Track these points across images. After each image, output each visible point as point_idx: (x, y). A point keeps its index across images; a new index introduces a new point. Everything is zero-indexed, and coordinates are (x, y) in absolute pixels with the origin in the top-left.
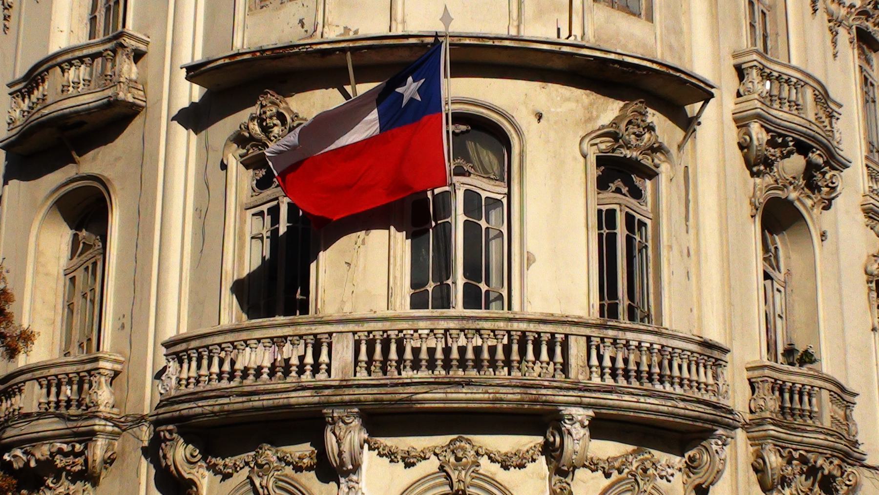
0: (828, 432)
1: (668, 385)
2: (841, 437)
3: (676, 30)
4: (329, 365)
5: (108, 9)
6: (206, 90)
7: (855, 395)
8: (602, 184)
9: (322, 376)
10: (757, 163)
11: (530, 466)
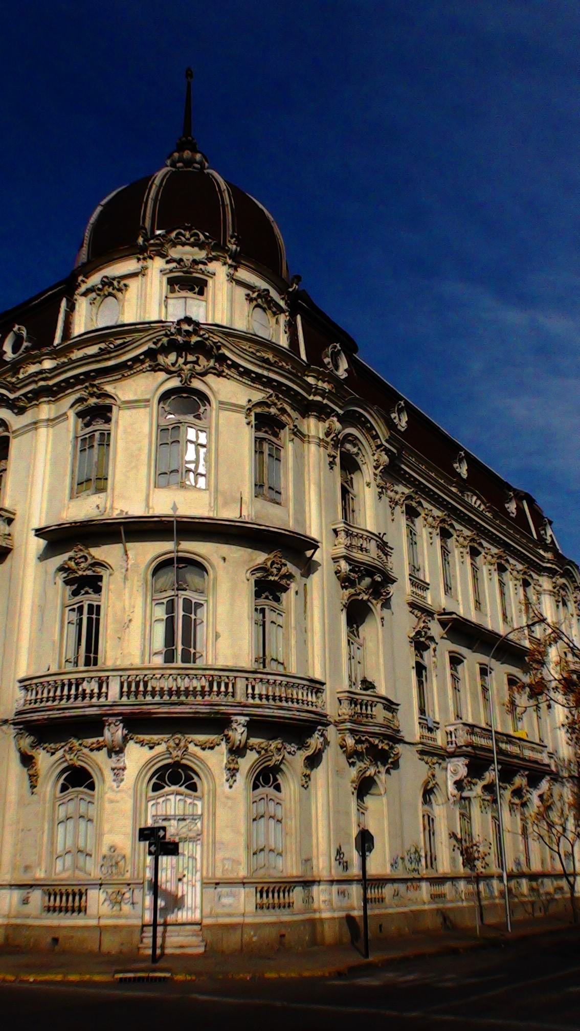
0: (382, 726)
1: (290, 703)
2: (388, 727)
4: (107, 693)
6: (46, 542)
7: (398, 705)
8: (258, 595)
9: (102, 700)
10: (346, 581)
11: (217, 748)
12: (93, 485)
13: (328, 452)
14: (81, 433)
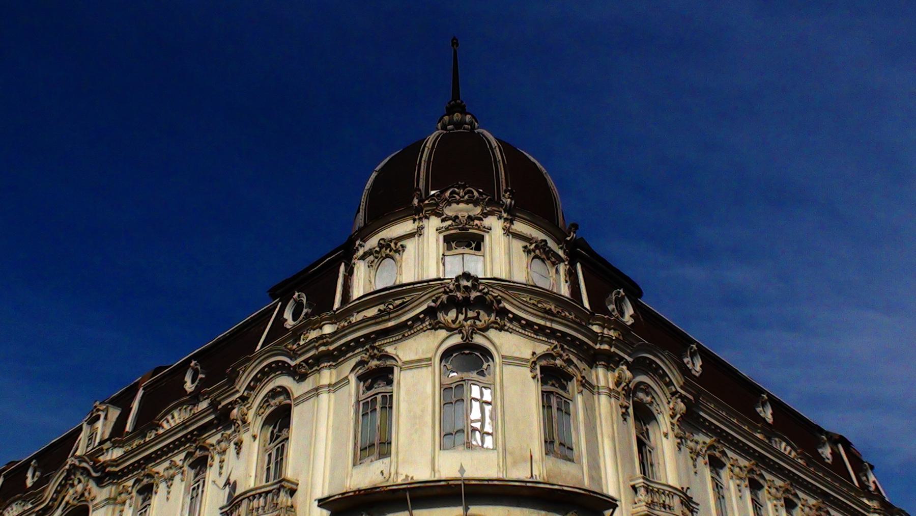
3: (595, 466)
5: (277, 463)
12: (376, 450)
13: (620, 402)
14: (362, 397)
